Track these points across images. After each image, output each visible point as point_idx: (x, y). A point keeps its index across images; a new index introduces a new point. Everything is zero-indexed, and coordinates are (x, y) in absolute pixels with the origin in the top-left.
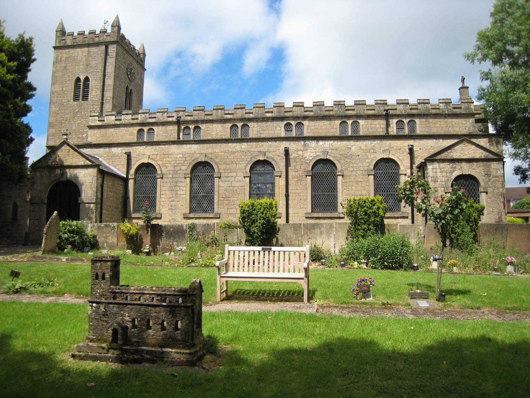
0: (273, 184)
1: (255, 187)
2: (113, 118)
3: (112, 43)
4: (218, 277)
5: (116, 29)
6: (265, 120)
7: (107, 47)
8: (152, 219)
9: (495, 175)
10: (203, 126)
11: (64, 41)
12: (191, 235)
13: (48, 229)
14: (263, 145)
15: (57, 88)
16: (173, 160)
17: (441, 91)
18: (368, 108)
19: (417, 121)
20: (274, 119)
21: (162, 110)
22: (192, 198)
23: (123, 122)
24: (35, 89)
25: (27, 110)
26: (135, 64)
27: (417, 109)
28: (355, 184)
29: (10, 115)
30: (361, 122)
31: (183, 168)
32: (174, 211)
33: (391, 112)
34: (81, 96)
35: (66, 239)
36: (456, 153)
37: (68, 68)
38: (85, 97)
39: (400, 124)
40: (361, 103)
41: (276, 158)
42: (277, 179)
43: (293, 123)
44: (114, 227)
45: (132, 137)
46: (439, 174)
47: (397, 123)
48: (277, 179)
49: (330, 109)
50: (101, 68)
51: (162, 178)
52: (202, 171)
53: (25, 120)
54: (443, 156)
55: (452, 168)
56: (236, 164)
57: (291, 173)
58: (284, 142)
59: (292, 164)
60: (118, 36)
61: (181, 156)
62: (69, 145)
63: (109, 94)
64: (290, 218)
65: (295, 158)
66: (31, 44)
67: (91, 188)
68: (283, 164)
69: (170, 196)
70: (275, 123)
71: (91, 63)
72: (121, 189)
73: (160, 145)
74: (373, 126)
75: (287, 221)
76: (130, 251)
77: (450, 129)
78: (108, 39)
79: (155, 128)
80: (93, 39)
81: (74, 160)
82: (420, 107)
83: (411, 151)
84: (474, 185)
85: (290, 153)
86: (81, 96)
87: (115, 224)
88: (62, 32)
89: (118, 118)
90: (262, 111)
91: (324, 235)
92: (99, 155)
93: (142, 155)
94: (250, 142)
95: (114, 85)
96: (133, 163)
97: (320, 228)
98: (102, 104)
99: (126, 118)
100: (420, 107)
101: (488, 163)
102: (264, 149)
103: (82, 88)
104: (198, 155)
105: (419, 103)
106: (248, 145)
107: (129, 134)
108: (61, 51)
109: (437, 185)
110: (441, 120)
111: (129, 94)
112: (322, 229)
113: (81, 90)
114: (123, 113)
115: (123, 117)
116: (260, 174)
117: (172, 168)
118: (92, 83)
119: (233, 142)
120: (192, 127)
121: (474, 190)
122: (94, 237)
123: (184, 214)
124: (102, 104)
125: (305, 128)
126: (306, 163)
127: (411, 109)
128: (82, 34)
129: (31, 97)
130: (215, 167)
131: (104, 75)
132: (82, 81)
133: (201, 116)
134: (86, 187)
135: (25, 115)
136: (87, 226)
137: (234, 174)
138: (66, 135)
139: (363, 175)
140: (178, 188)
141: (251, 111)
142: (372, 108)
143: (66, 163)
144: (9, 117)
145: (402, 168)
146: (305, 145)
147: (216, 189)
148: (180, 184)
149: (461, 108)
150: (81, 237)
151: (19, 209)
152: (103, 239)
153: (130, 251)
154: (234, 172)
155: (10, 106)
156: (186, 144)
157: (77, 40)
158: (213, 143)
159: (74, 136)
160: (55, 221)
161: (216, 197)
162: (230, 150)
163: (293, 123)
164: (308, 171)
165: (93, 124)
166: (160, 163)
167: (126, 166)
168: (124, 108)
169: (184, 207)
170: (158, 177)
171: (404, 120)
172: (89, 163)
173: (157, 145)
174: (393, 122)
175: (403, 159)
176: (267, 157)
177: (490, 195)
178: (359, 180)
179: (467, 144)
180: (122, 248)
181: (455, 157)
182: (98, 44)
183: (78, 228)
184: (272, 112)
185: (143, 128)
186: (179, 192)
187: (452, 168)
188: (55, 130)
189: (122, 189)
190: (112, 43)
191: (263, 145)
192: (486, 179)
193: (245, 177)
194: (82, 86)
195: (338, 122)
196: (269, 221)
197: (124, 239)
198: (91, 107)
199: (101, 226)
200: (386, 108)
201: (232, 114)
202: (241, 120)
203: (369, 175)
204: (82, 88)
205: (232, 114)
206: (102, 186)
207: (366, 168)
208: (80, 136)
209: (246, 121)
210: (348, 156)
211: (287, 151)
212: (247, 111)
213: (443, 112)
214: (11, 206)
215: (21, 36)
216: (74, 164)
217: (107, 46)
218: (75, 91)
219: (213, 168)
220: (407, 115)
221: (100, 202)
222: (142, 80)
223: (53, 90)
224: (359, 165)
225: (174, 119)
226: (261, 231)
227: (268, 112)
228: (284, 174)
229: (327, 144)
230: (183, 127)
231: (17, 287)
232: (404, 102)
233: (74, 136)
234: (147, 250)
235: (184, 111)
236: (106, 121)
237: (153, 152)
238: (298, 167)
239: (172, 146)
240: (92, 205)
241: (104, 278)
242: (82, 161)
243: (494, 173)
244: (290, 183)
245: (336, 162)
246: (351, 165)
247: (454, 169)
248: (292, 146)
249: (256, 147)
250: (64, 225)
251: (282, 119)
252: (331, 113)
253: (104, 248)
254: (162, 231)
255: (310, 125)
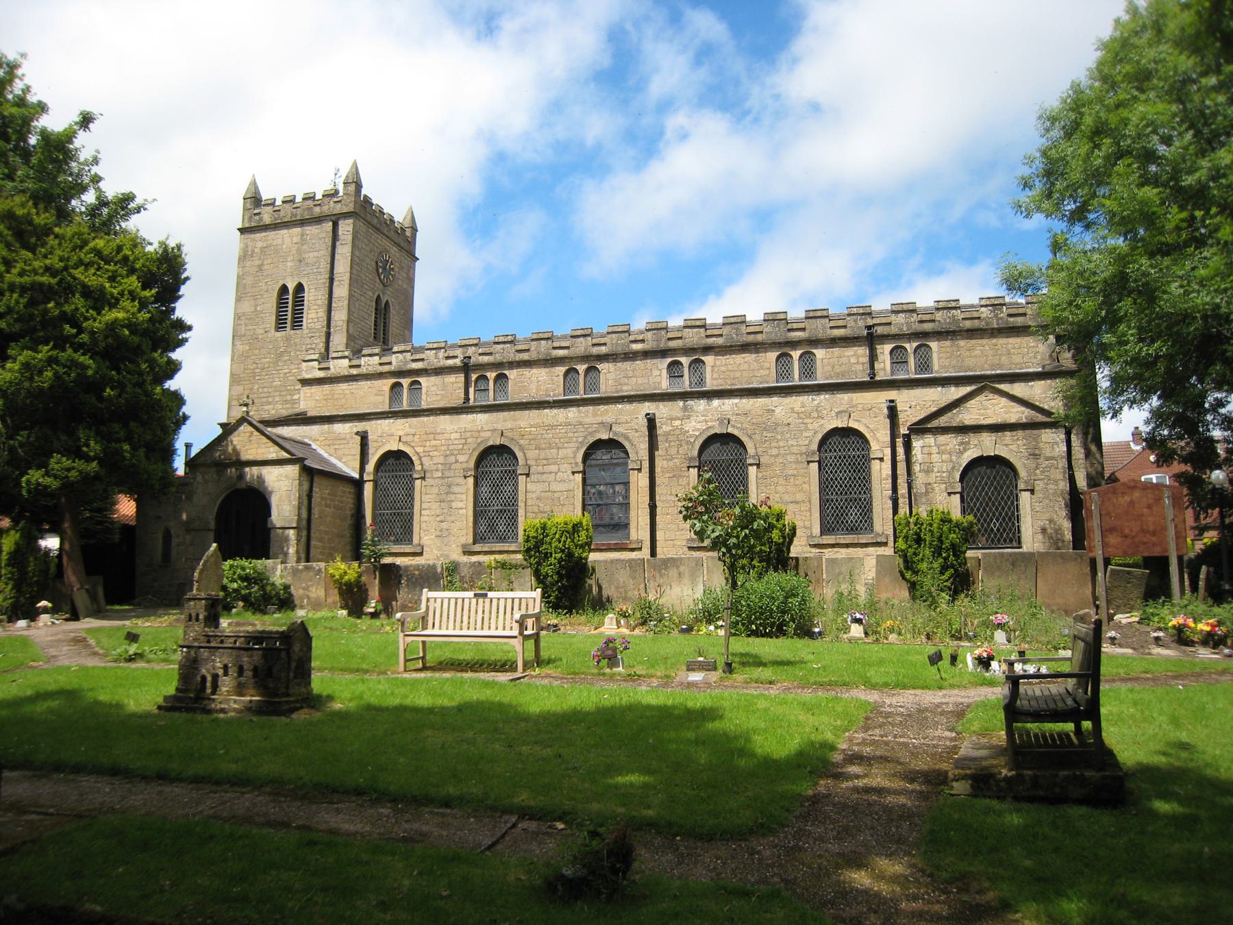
0: (626, 484)
1: (593, 491)
2: (346, 362)
3: (346, 215)
4: (401, 635)
5: (352, 188)
6: (630, 356)
7: (335, 225)
8: (383, 555)
9: (1048, 455)
10: (512, 374)
11: (257, 218)
12: (450, 582)
13: (201, 573)
14: (607, 411)
15: (247, 307)
16: (444, 444)
17: (971, 287)
18: (832, 324)
19: (934, 345)
20: (646, 354)
21: (435, 346)
22: (477, 515)
23: (363, 370)
24: (190, 328)
25: (173, 368)
26: (394, 250)
27: (933, 321)
28: (781, 481)
29: (144, 381)
30: (819, 353)
31: (462, 458)
32: (446, 540)
33: (880, 330)
34: (289, 321)
35: (235, 591)
36: (971, 414)
37: (266, 267)
38: (297, 323)
39: (898, 356)
40: (819, 314)
41: (631, 434)
42: (633, 474)
43: (685, 361)
44: (320, 570)
45: (380, 399)
46: (935, 458)
47: (891, 352)
48: (634, 476)
49: (758, 329)
50: (325, 265)
51: (423, 478)
52: (495, 462)
53: (171, 385)
54: (942, 421)
55: (962, 443)
56: (558, 449)
57: (660, 464)
58: (647, 404)
59: (662, 445)
60: (356, 202)
61: (457, 436)
62: (251, 424)
63: (340, 316)
64: (659, 550)
65: (667, 434)
66: (180, 256)
67: (290, 501)
68: (644, 446)
69: (438, 512)
70: (649, 362)
71: (306, 256)
72: (349, 501)
73: (420, 416)
74: (844, 360)
75: (653, 553)
76: (345, 612)
77: (1003, 358)
78: (339, 209)
79: (422, 380)
80: (309, 209)
81: (260, 451)
82: (939, 316)
83: (893, 412)
84: (1007, 477)
85: (658, 425)
86: (289, 321)
87: (322, 565)
88: (254, 200)
89: (355, 362)
90: (624, 339)
91: (686, 581)
92: (311, 438)
93: (388, 435)
94: (583, 405)
95: (351, 296)
96: (371, 451)
97: (678, 567)
98: (328, 335)
99: (370, 363)
100: (939, 316)
101: (1035, 432)
102: (609, 419)
103: (290, 305)
104: (488, 434)
105: (938, 309)
106: (580, 412)
107: (374, 395)
108: (252, 236)
109: (932, 478)
110: (984, 341)
111: (382, 311)
112: (682, 568)
113: (290, 309)
114: (364, 352)
115: (363, 361)
116: (603, 467)
117: (441, 460)
118: (308, 296)
119: (551, 407)
120: (492, 375)
121: (1008, 487)
122: (286, 587)
123: (464, 546)
124: (328, 335)
125: (708, 369)
126: (688, 443)
127: (921, 322)
128: (290, 201)
129: (181, 343)
130: (519, 454)
131: (332, 280)
132: (291, 291)
133: (509, 353)
134: (280, 499)
135: (171, 377)
136: (274, 569)
137: (554, 468)
138: (246, 405)
139: (797, 462)
140: (452, 497)
141: (603, 340)
142: (840, 323)
143: (245, 456)
144: (141, 385)
145: (874, 446)
146: (685, 409)
147: (521, 497)
148: (456, 489)
149: (1024, 315)
150: (263, 588)
151: (175, 541)
152: (301, 591)
153: (345, 612)
154: (555, 463)
155: (144, 366)
156: (467, 413)
157: (282, 213)
158: (514, 410)
159: (277, 399)
160: (213, 559)
161: (521, 512)
162: (547, 422)
163: (685, 361)
164: (691, 459)
165: (308, 376)
166: (420, 450)
167: (358, 457)
168: (371, 339)
169: (464, 532)
170: (415, 476)
171: (907, 346)
172: (286, 455)
173: (415, 416)
174: (885, 350)
175: (877, 429)
176: (615, 434)
177: (1038, 495)
178: (791, 472)
179: (991, 396)
180: (332, 607)
181: (967, 423)
182: (318, 220)
183: (255, 571)
184: (643, 341)
185: (401, 380)
186: (454, 505)
187: (962, 443)
188: (241, 388)
189: (351, 501)
190: (346, 215)
191: (607, 411)
192: (1031, 463)
193: (573, 473)
194: (290, 301)
195: (772, 356)
196: (570, 555)
197: (336, 591)
198: (309, 341)
199: (298, 570)
200: (870, 322)
201: (567, 348)
202: (585, 358)
203: (809, 462)
204: (290, 305)
205: (567, 348)
206: (310, 497)
207: (804, 449)
208: (289, 398)
209: (595, 361)
210: (770, 427)
211: (651, 422)
212: (595, 341)
213: (987, 324)
214: (160, 536)
215: (163, 244)
216: (260, 458)
217: (335, 221)
218: (278, 312)
219: (515, 457)
220: (912, 334)
221: (306, 526)
222: (411, 281)
223: (239, 311)
224: (790, 442)
225: (458, 362)
226: (558, 573)
227: (635, 341)
228: (646, 465)
229: (729, 404)
230: (474, 377)
231: (131, 652)
232: (905, 307)
233: (277, 399)
234: (372, 610)
235: (476, 345)
236: (332, 370)
237: (408, 430)
238: (673, 451)
239: (442, 417)
240: (292, 532)
241: (197, 619)
242: (273, 453)
243: (1047, 452)
244: (658, 481)
245: (744, 439)
246: (773, 444)
247: (965, 446)
248: (661, 410)
249: (595, 415)
250: (231, 566)
251: (663, 353)
252: (759, 338)
253: (302, 607)
254: (401, 576)
255: (718, 363)
